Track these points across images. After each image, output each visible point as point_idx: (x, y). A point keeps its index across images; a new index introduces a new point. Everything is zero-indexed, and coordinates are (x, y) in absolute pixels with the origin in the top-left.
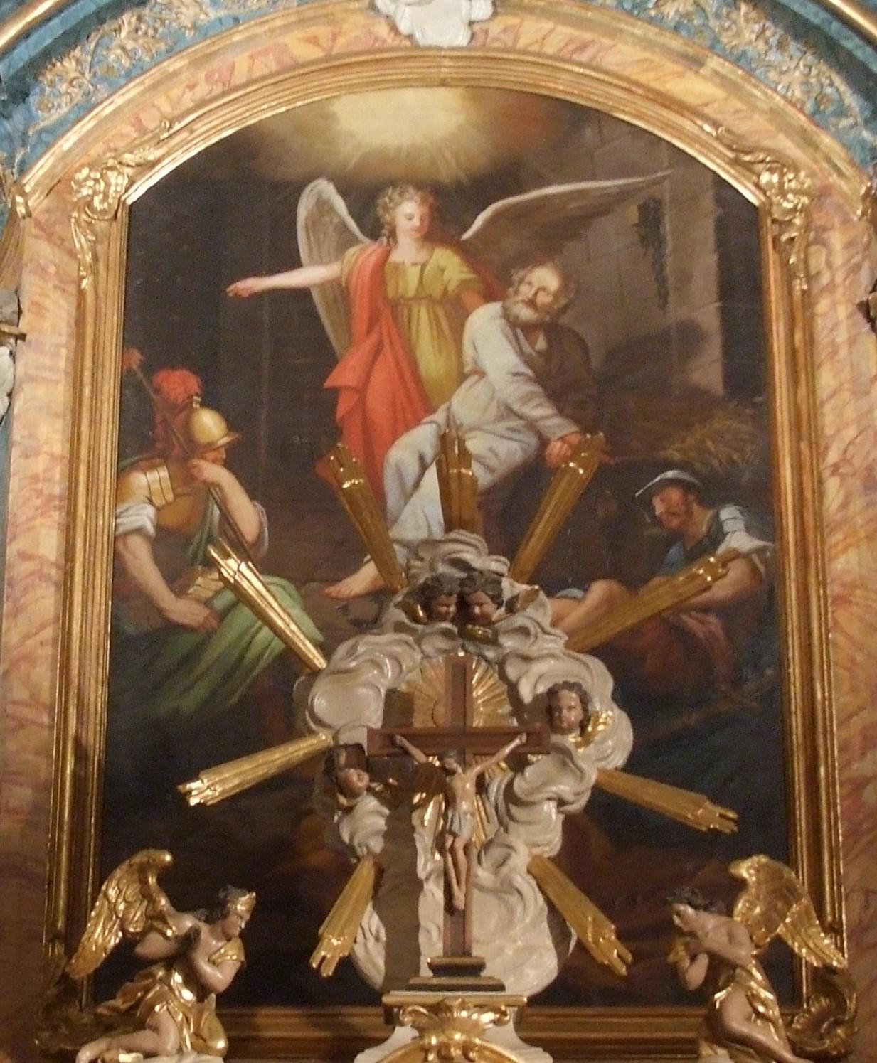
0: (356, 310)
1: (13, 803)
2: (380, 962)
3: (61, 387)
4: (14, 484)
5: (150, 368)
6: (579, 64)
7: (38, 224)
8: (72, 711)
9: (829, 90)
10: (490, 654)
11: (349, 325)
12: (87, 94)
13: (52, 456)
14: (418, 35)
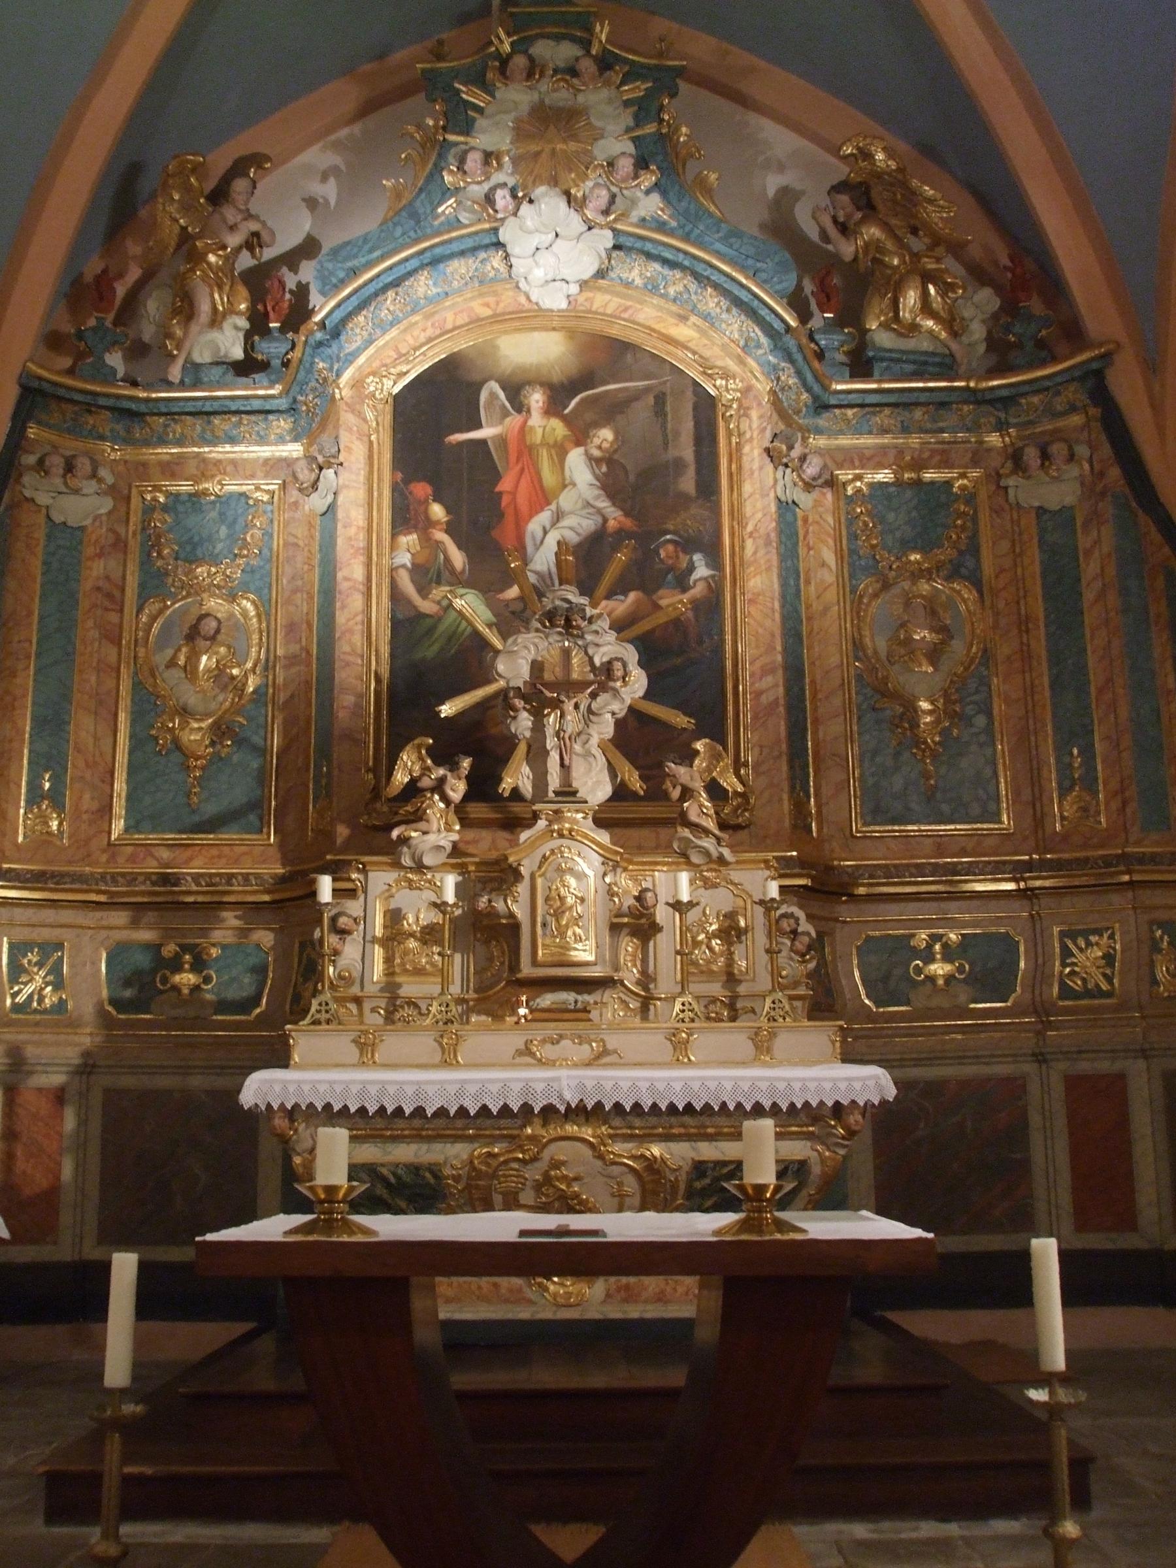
0: (511, 451)
1: (345, 704)
2: (530, 790)
3: (361, 491)
4: (340, 541)
5: (407, 481)
6: (624, 320)
7: (347, 404)
8: (373, 658)
9: (752, 334)
10: (580, 643)
11: (507, 458)
12: (370, 334)
13: (358, 527)
14: (541, 303)
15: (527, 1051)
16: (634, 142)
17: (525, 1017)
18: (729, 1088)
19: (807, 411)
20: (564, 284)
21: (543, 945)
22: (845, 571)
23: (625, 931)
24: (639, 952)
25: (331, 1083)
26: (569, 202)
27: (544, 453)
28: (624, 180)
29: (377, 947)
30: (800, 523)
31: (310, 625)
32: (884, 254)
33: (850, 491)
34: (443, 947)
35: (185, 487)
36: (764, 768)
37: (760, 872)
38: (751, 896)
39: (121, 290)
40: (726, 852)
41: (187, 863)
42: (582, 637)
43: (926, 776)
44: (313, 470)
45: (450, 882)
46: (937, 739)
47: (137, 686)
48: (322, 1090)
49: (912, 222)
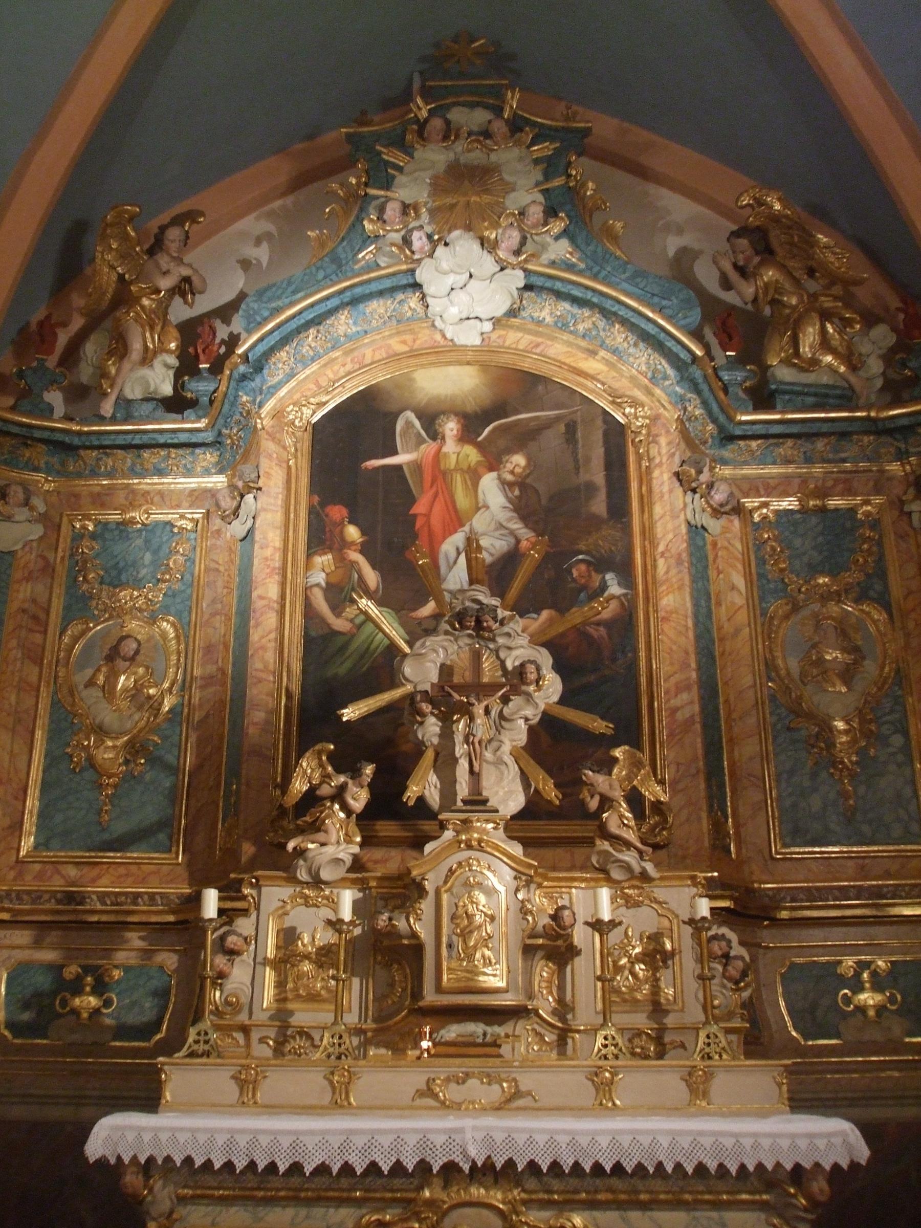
1: (255, 720)
3: (279, 514)
5: (323, 504)
6: (536, 354)
7: (268, 433)
8: (285, 674)
9: (659, 367)
13: (275, 548)
14: (456, 340)
15: (428, 1092)
16: (543, 195)
17: (428, 1050)
18: (666, 1145)
19: (713, 442)
20: (477, 322)
21: (449, 969)
22: (755, 594)
23: (540, 954)
24: (555, 977)
25: (194, 1131)
26: (482, 245)
27: (458, 478)
28: (535, 226)
29: (268, 969)
30: (709, 547)
31: (226, 646)
32: (781, 294)
33: (756, 518)
34: (338, 970)
35: (114, 517)
36: (680, 786)
37: (686, 889)
38: (677, 916)
39: (63, 338)
40: (649, 867)
41: (93, 881)
42: (493, 640)
43: (844, 795)
44: (234, 498)
45: (347, 898)
46: (854, 759)
47: (56, 704)
48: (182, 1141)
49: (810, 263)
